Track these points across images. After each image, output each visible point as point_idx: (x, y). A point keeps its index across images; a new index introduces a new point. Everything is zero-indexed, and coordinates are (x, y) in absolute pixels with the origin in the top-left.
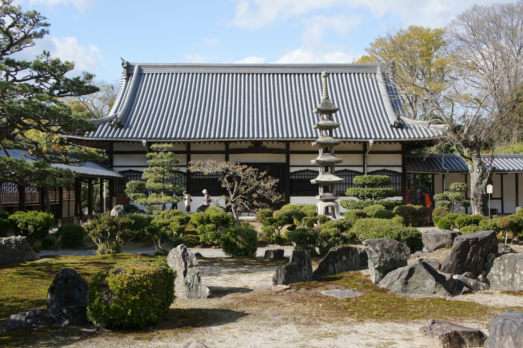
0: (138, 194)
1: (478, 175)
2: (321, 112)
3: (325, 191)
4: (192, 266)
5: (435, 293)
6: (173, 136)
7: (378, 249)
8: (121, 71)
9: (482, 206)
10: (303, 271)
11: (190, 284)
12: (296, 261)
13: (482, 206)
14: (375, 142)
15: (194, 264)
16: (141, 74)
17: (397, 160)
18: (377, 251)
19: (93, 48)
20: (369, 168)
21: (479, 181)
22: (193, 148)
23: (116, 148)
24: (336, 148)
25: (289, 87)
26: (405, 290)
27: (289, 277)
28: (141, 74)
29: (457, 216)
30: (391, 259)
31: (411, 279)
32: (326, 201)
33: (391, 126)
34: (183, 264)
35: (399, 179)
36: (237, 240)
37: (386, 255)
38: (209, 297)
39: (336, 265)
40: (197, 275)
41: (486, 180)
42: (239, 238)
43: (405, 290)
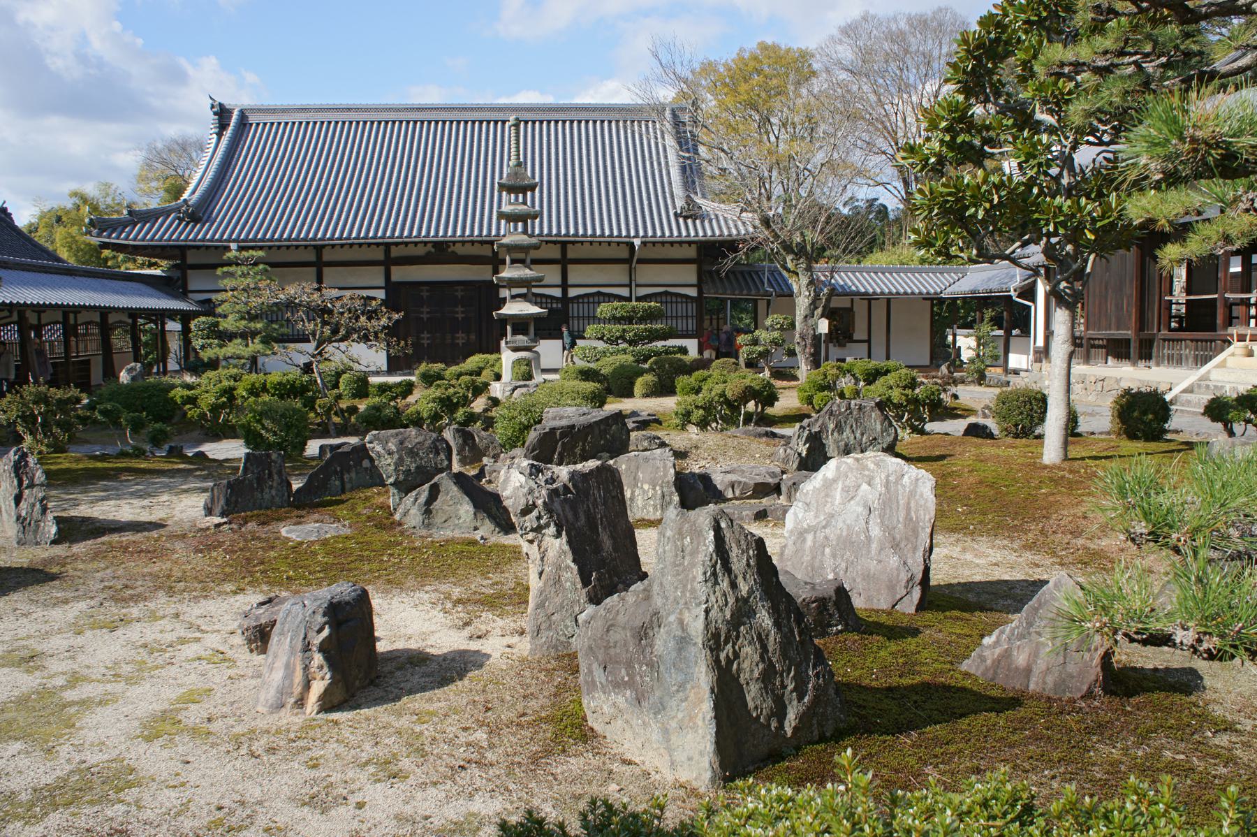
0: (209, 341)
1: (807, 302)
2: (511, 189)
3: (514, 333)
4: (31, 486)
5: (476, 529)
6: (337, 235)
7: (394, 448)
8: (211, 118)
9: (812, 355)
10: (267, 490)
11: (25, 519)
12: (253, 473)
13: (812, 355)
14: (644, 244)
15: (37, 481)
16: (243, 123)
17: (689, 274)
18: (390, 453)
19: (251, 78)
20: (639, 289)
21: (808, 312)
22: (327, 256)
23: (192, 258)
24: (534, 254)
25: (607, 142)
26: (429, 524)
27: (236, 502)
28: (243, 123)
29: (710, 376)
30: (417, 467)
31: (436, 505)
32: (516, 349)
33: (676, 214)
34: (16, 482)
35: (692, 309)
36: (264, 427)
37: (408, 460)
38: (54, 542)
39: (346, 477)
40: (41, 501)
41: (819, 311)
42: (267, 422)
43: (429, 524)
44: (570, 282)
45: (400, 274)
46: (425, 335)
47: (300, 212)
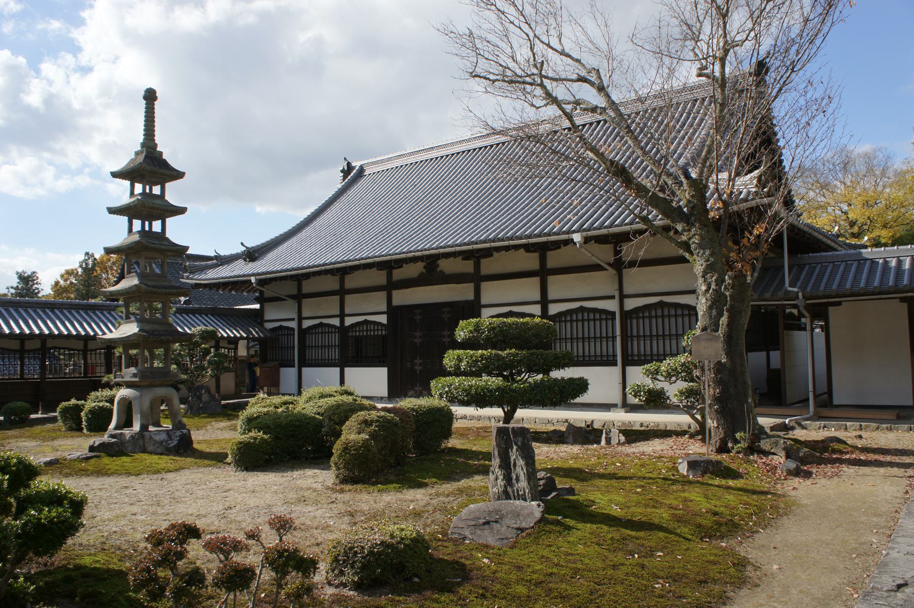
44: (551, 296)
45: (402, 297)
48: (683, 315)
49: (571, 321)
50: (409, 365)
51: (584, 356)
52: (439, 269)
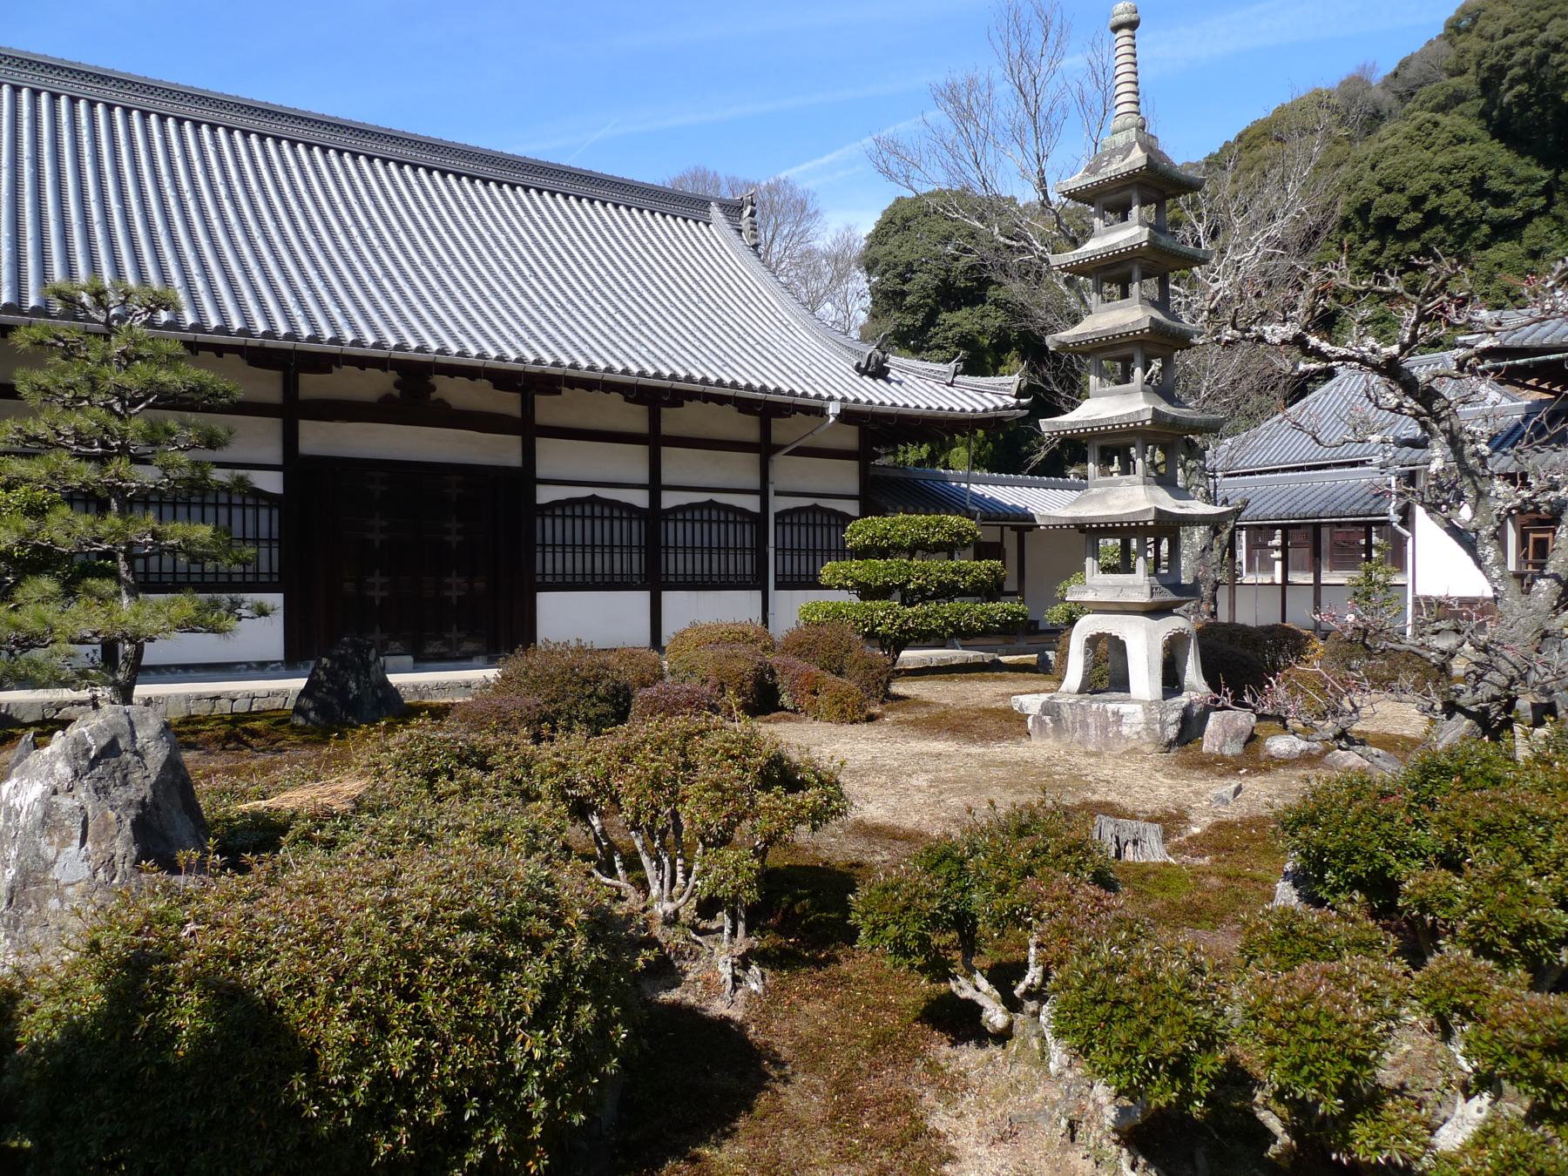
44: (666, 479)
45: (318, 438)
46: (377, 579)
47: (636, 263)
48: (621, 519)
49: (792, 524)
50: (349, 587)
51: (593, 574)
52: (434, 396)
